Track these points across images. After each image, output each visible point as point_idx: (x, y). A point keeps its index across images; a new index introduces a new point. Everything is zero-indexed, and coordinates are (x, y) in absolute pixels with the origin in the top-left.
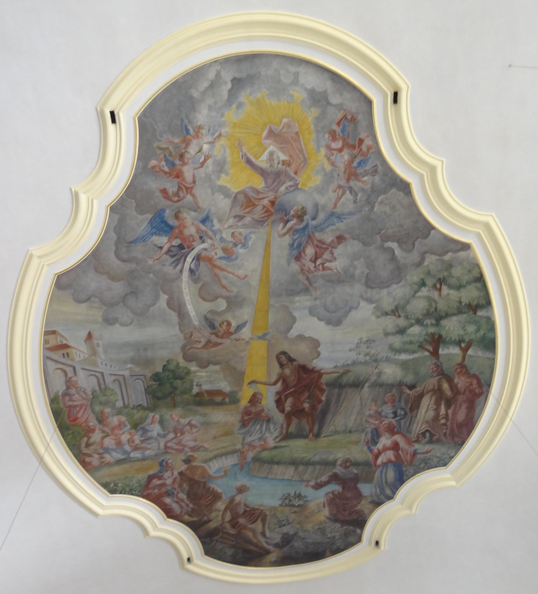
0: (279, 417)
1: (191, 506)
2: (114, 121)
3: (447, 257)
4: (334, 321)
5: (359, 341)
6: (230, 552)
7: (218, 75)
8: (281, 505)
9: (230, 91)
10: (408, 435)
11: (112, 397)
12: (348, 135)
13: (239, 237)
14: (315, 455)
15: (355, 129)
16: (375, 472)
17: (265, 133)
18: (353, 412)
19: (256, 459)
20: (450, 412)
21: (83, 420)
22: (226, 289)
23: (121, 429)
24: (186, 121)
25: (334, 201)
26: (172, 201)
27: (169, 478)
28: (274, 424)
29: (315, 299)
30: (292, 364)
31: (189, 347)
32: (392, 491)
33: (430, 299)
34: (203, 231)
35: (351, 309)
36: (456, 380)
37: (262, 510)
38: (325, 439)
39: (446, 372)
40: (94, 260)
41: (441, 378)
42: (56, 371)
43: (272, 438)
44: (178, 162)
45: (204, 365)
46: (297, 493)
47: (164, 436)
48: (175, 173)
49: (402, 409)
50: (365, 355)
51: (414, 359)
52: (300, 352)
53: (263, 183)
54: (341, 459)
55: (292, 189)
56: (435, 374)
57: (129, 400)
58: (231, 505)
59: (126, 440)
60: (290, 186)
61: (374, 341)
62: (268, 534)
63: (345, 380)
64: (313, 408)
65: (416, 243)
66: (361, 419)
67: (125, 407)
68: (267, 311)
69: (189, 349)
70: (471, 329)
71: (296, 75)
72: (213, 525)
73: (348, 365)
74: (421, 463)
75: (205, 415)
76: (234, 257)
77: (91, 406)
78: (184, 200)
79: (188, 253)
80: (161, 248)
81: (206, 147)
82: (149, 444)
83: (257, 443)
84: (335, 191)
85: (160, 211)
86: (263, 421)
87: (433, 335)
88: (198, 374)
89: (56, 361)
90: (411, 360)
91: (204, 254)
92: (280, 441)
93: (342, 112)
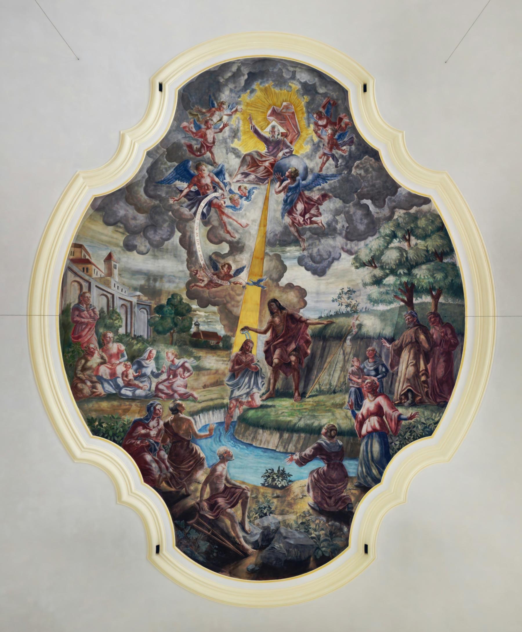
0: (267, 370)
1: (171, 470)
2: (161, 89)
3: (413, 210)
4: (319, 267)
5: (341, 291)
6: (204, 546)
7: (239, 69)
8: (263, 485)
9: (246, 81)
10: (390, 396)
11: (116, 322)
12: (331, 116)
13: (244, 190)
14: (300, 420)
15: (336, 111)
16: (360, 445)
17: (269, 112)
18: (337, 368)
19: (242, 419)
20: (429, 366)
21: (86, 340)
22: (230, 234)
23: (118, 358)
24: (213, 98)
25: (320, 165)
26: (195, 154)
27: (154, 428)
28: (263, 378)
29: (304, 250)
30: (281, 312)
31: (193, 284)
32: (378, 469)
33: (400, 250)
34: (216, 182)
35: (334, 259)
36: (432, 331)
37: (244, 489)
38: (310, 399)
39: (421, 323)
40: (127, 193)
41: (417, 329)
42: (73, 283)
43: (259, 395)
44: (203, 126)
45: (203, 304)
46: (281, 469)
47: (157, 376)
48: (200, 134)
49: (383, 365)
50: (347, 306)
51: (390, 310)
52: (289, 299)
53: (266, 149)
54: (325, 427)
55: (287, 155)
56: (411, 325)
57: (131, 328)
58: (212, 478)
59: (121, 372)
60: (287, 153)
61: (354, 292)
62: (247, 527)
63: (329, 331)
64: (299, 361)
65: (387, 200)
66: (345, 376)
67: (127, 335)
68: (263, 259)
69: (193, 286)
70: (439, 276)
71: (294, 73)
72: (191, 502)
73: (331, 315)
74: (406, 432)
75: (198, 358)
76: (239, 207)
77: (96, 326)
78: (205, 156)
79: (203, 199)
80: (181, 191)
81: (225, 118)
82: (142, 382)
83: (244, 399)
84: (320, 158)
85: (185, 161)
86: (253, 372)
87: (406, 284)
88: (198, 312)
89: (76, 274)
90: (388, 311)
91: (215, 201)
92: (267, 399)
93: (326, 99)
